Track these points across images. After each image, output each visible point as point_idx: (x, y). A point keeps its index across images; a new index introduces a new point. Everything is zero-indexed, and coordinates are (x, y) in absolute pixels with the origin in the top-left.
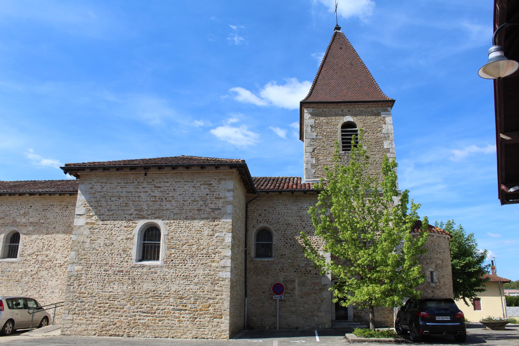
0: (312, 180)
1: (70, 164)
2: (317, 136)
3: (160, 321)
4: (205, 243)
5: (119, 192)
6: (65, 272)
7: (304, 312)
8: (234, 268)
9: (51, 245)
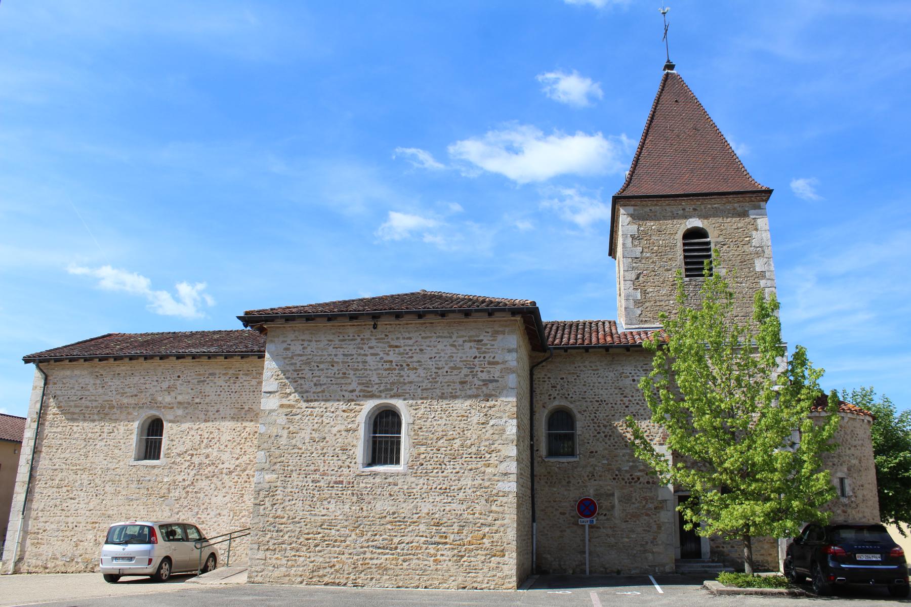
0: (637, 326)
1: (252, 312)
2: (642, 252)
3: (404, 561)
4: (475, 437)
5: (331, 355)
6: (237, 482)
9: (214, 438)
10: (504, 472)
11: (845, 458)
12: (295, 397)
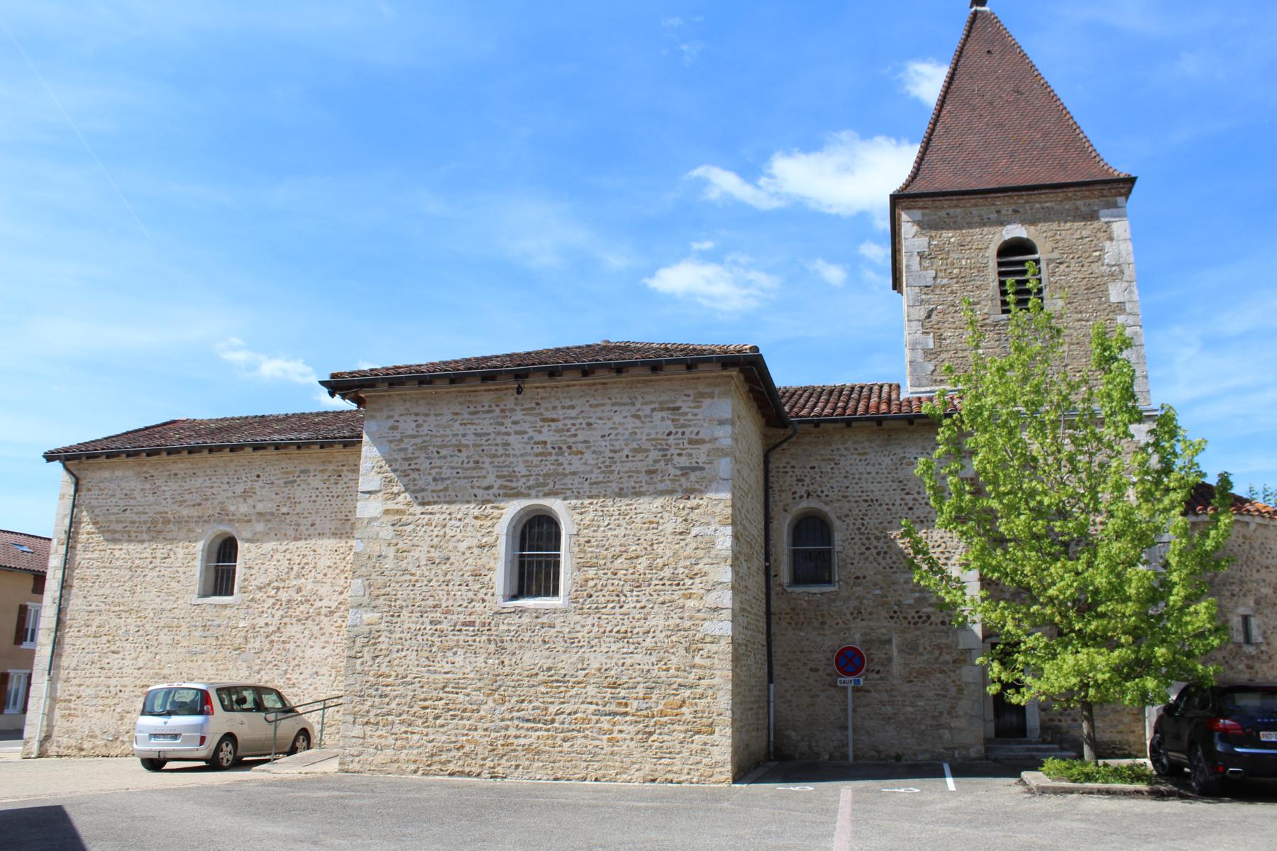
0: (928, 389)
1: (342, 374)
2: (935, 278)
3: (565, 740)
4: (669, 553)
6: (341, 627)
9: (307, 564)
10: (714, 606)
12: (406, 498)
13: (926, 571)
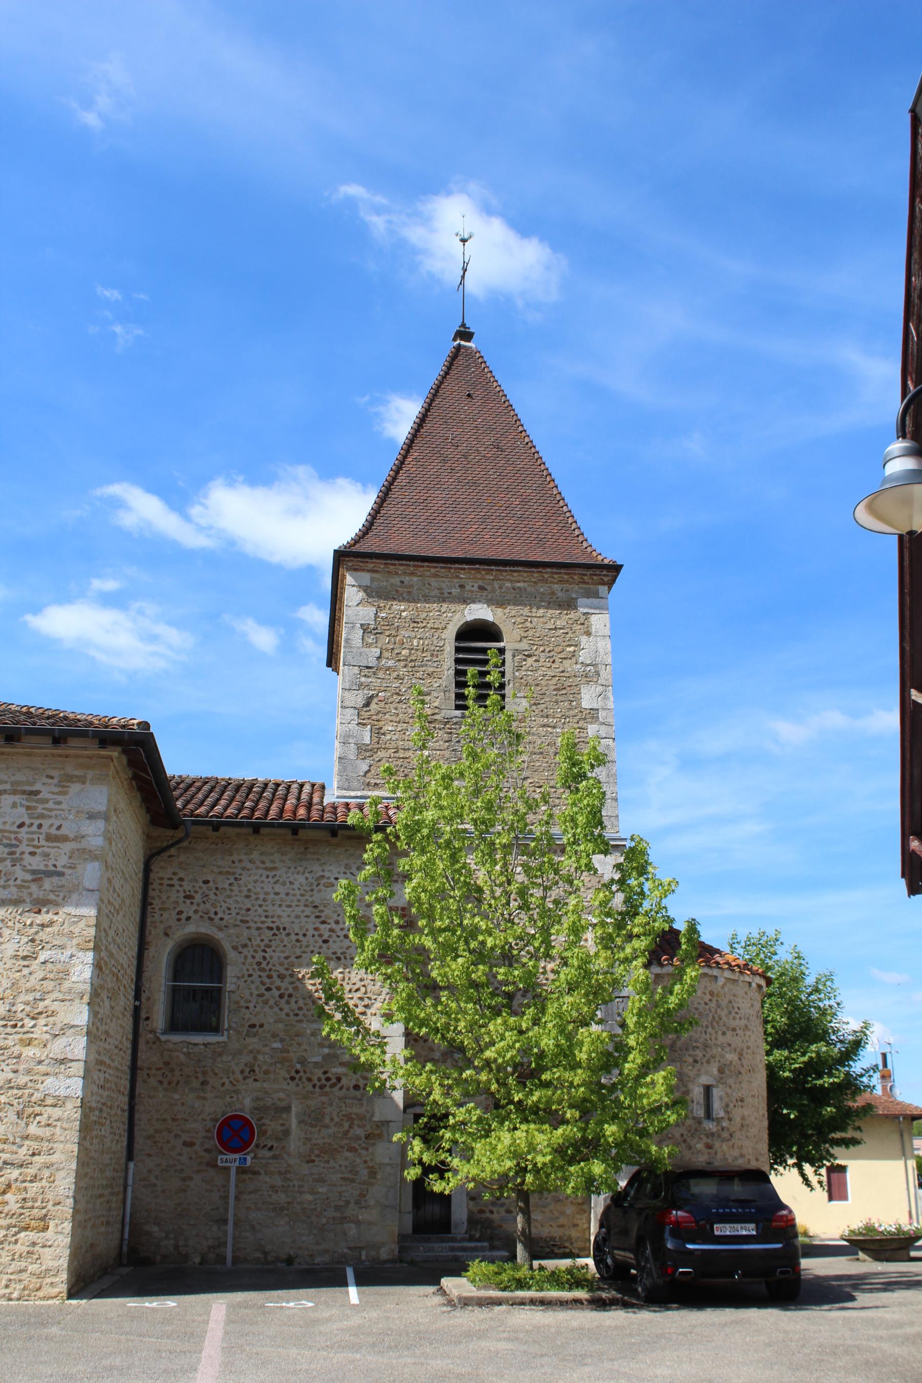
0: (359, 793)
2: (379, 658)
7: (315, 1209)
8: (96, 1064)
11: (714, 1051)
13: (339, 1022)
